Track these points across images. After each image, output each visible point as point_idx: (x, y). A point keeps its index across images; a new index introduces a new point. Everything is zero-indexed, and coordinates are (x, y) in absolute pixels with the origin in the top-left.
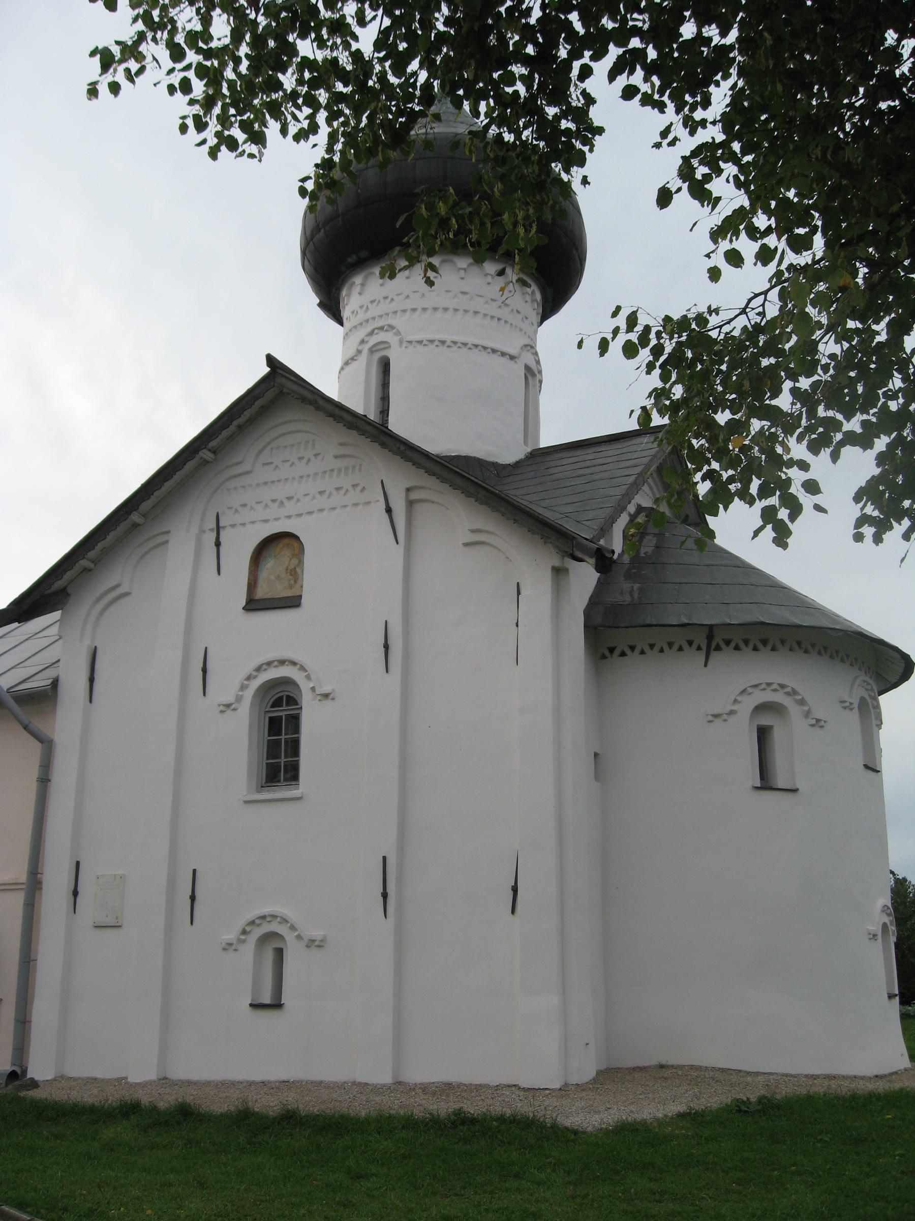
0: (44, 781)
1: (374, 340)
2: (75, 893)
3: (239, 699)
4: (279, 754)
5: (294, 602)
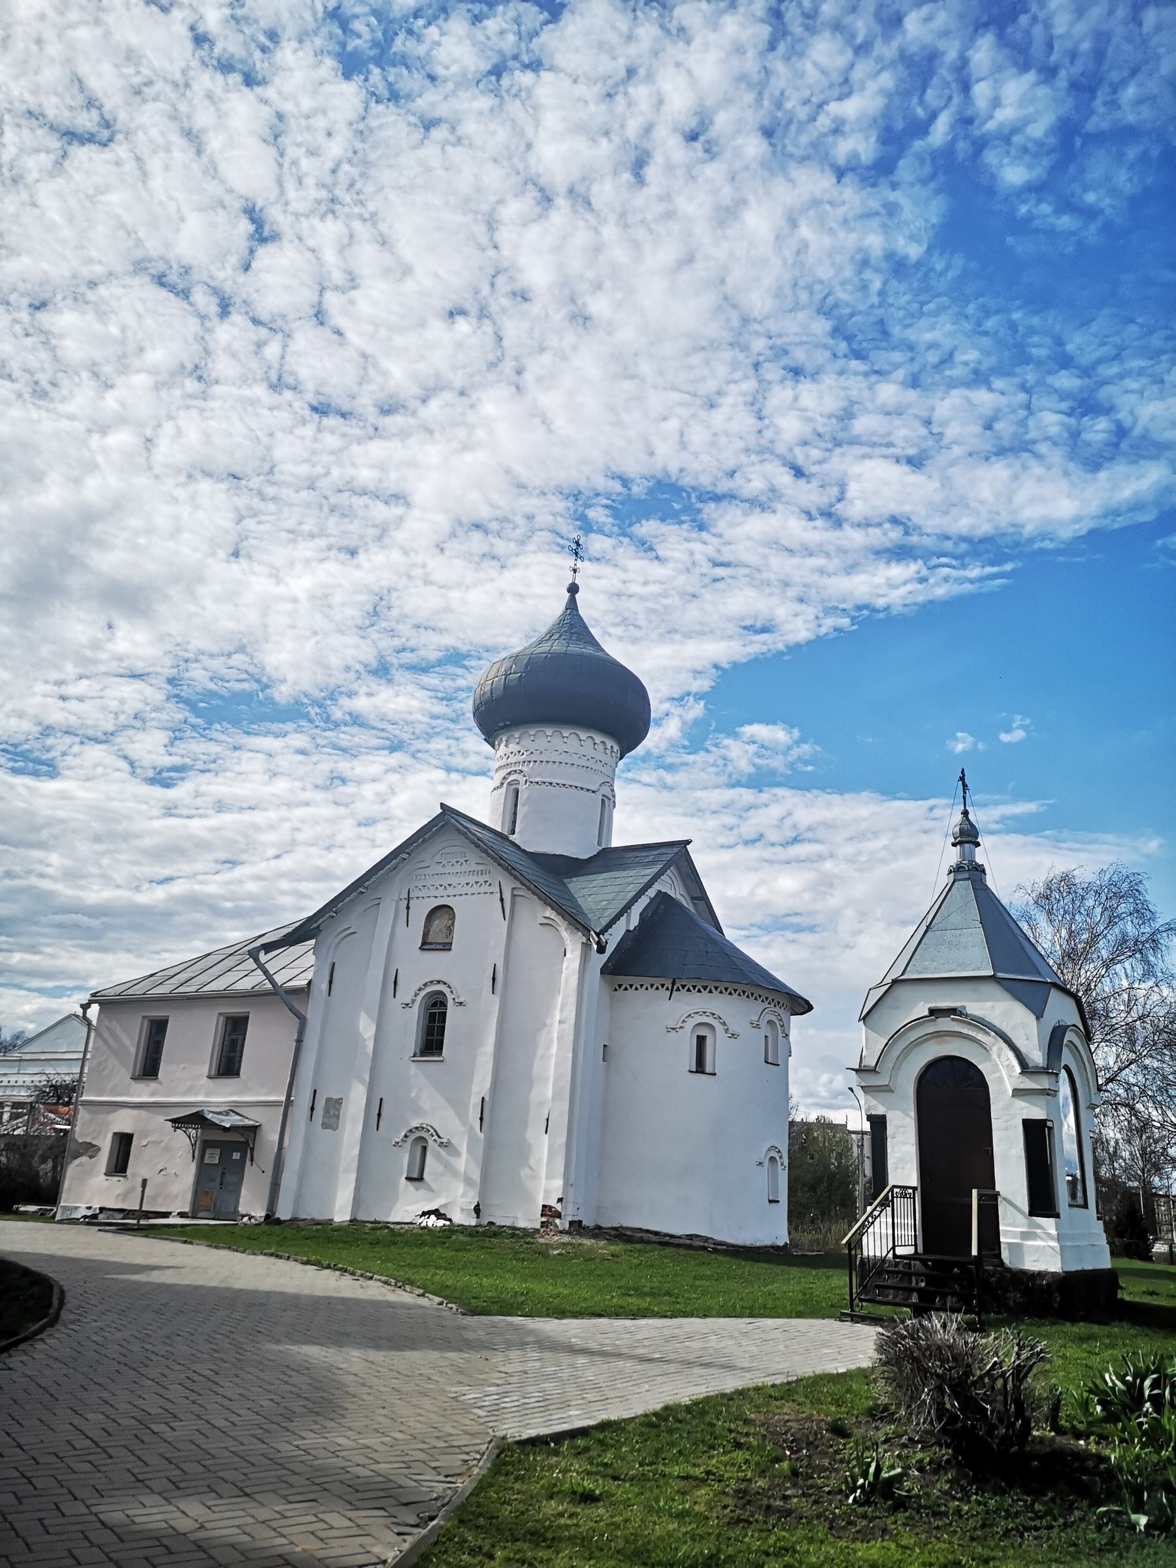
0: (299, 1041)
1: (511, 778)
3: (413, 1001)
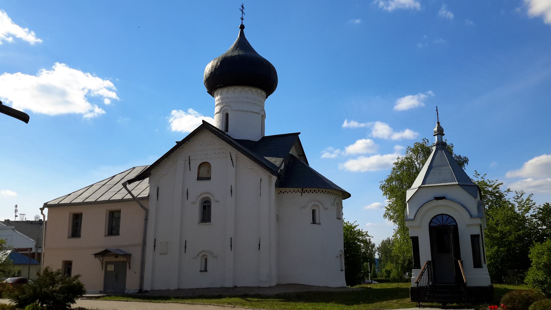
0: (146, 219)
2: (155, 246)
4: (206, 214)
5: (209, 179)
